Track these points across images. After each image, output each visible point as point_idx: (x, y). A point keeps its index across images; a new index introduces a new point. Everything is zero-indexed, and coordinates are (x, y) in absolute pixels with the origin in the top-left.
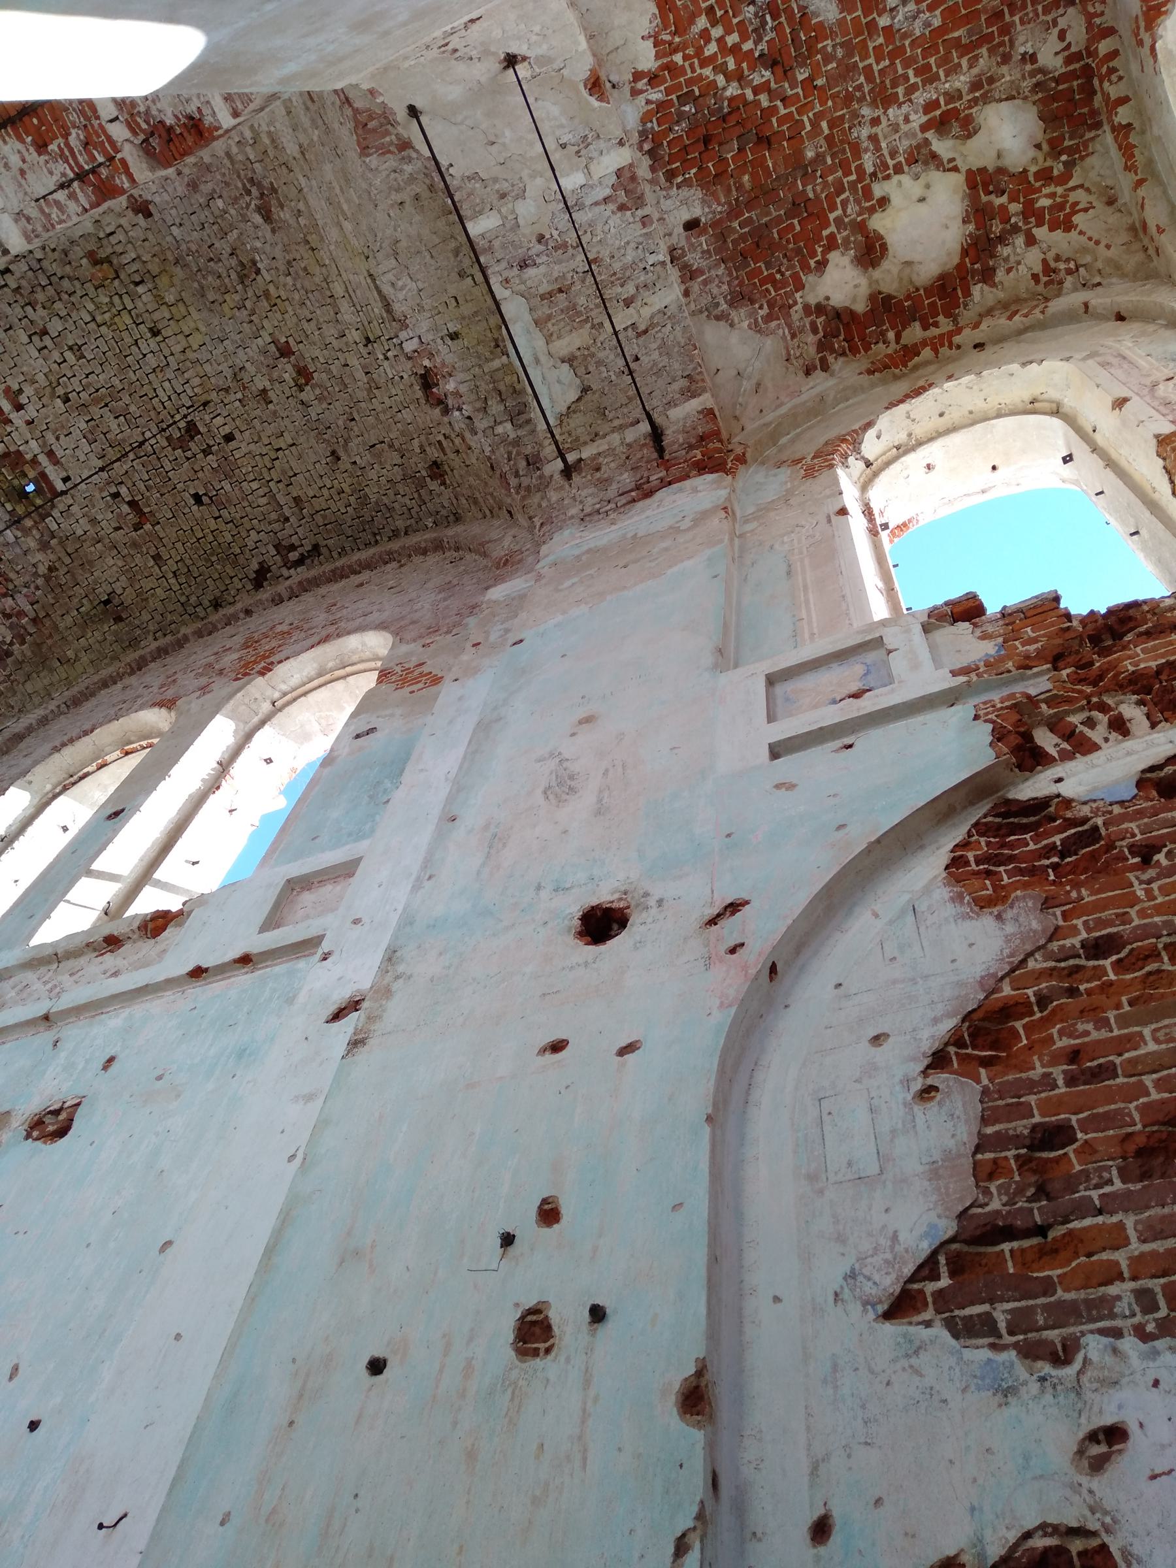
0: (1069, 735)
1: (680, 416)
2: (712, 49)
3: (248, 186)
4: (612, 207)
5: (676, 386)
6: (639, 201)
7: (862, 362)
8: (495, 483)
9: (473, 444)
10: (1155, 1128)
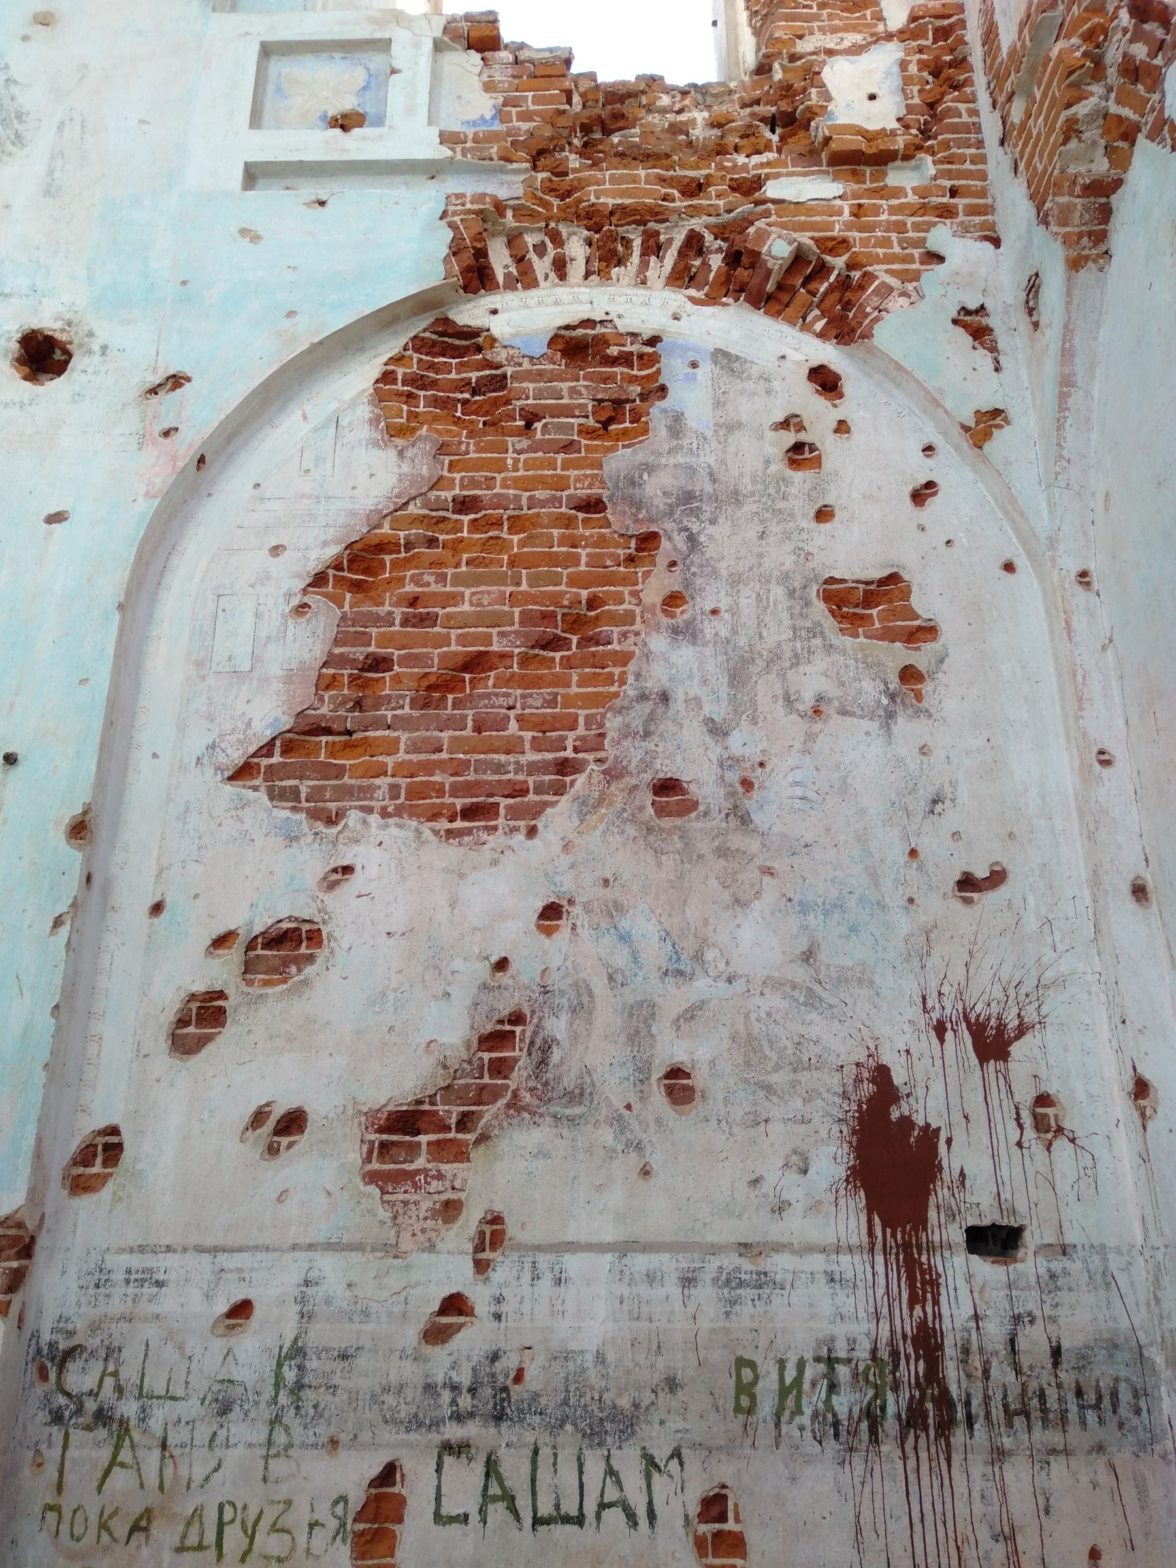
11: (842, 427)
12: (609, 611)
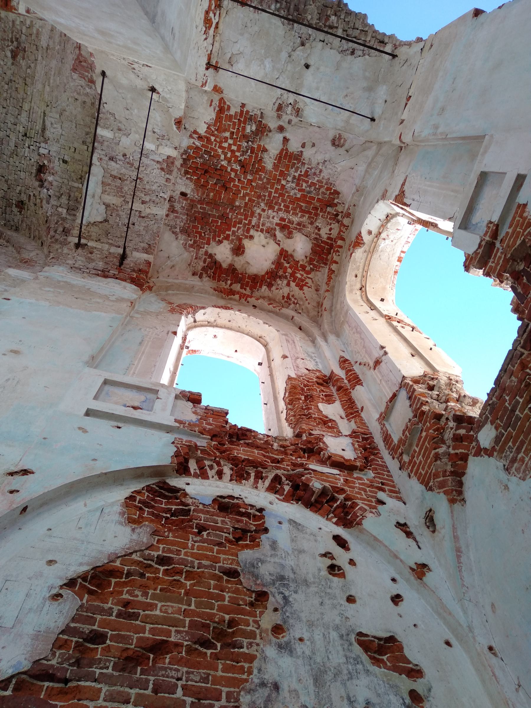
0: (201, 468)
1: (137, 257)
2: (225, 145)
3: (14, 39)
4: (159, 166)
5: (142, 245)
6: (170, 172)
7: (214, 284)
8: (44, 228)
9: (44, 207)
10: (138, 649)
11: (352, 562)
12: (241, 629)
